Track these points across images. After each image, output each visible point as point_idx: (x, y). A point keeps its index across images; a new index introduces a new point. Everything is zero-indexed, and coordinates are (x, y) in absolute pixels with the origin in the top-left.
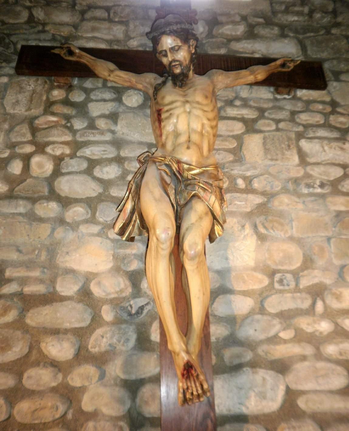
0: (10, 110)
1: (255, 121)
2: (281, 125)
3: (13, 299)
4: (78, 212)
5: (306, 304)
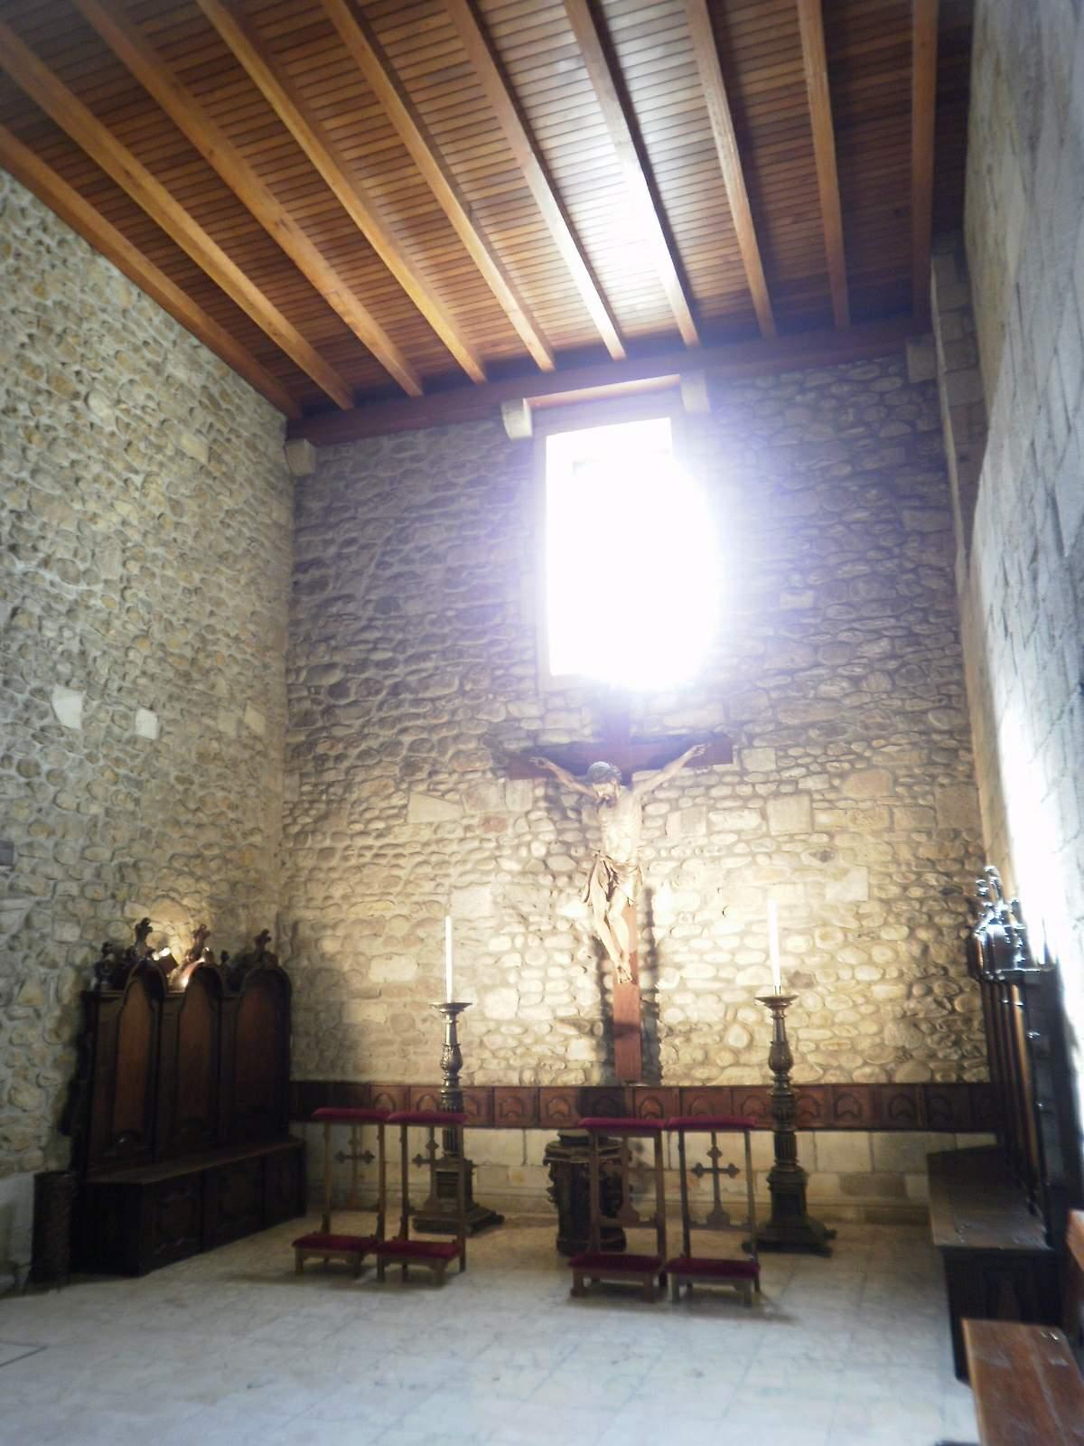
0: (511, 808)
1: (677, 800)
2: (698, 801)
3: (879, 938)
4: (563, 881)
5: (698, 931)
